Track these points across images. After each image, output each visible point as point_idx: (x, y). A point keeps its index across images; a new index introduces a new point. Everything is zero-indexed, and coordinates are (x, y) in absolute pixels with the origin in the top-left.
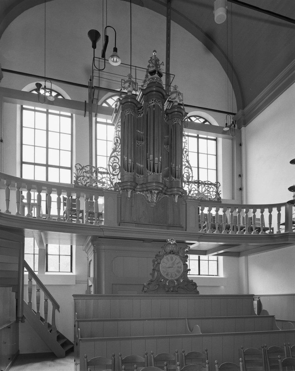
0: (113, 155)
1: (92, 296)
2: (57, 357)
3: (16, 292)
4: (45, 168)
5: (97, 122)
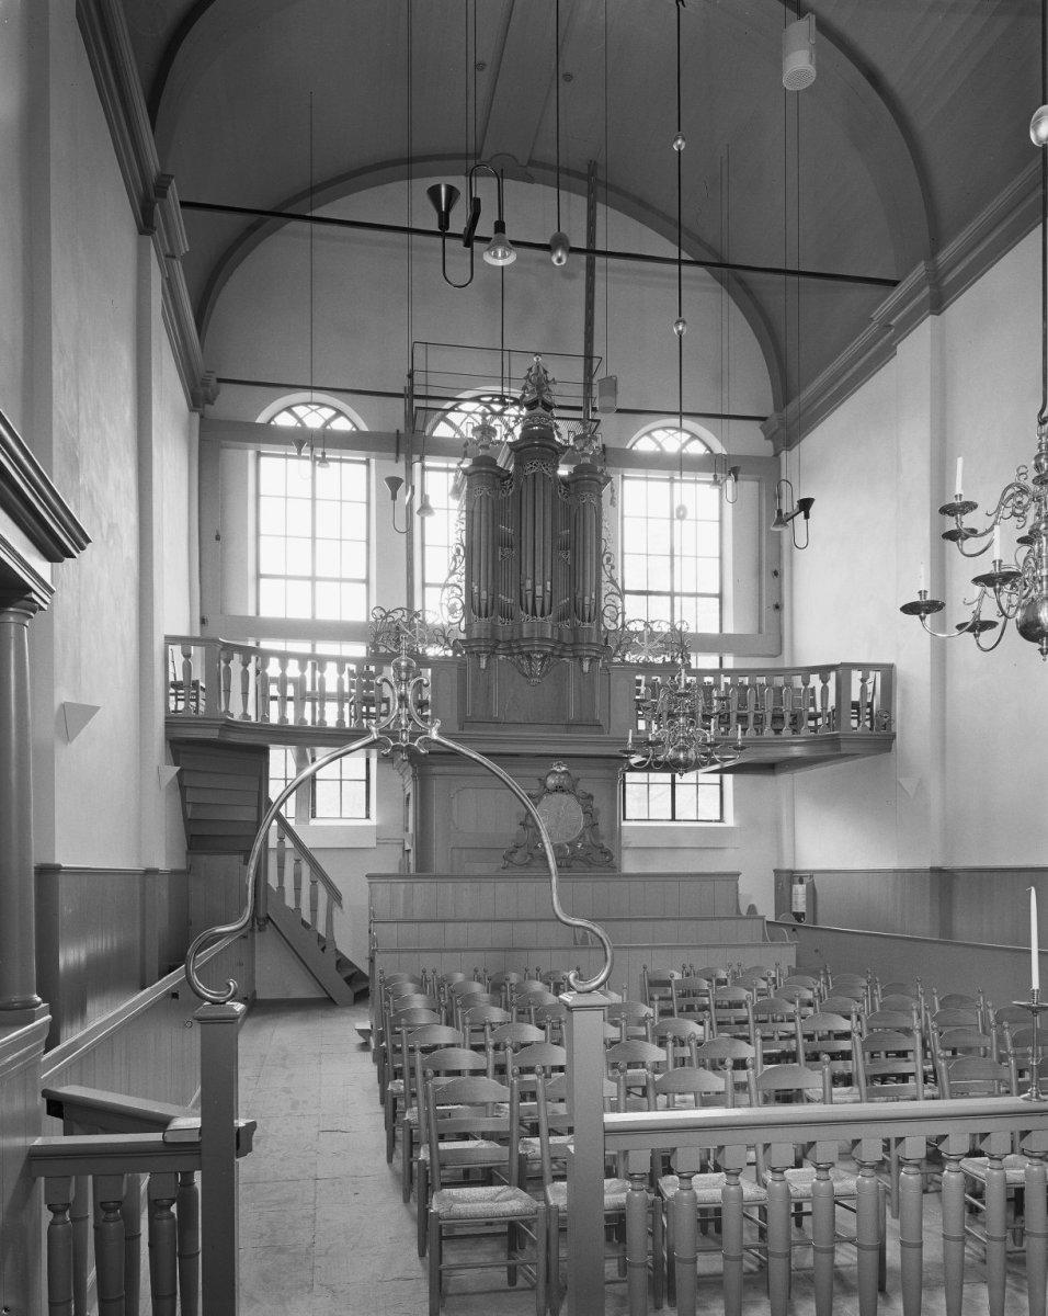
1: (410, 876)
2: (335, 1003)
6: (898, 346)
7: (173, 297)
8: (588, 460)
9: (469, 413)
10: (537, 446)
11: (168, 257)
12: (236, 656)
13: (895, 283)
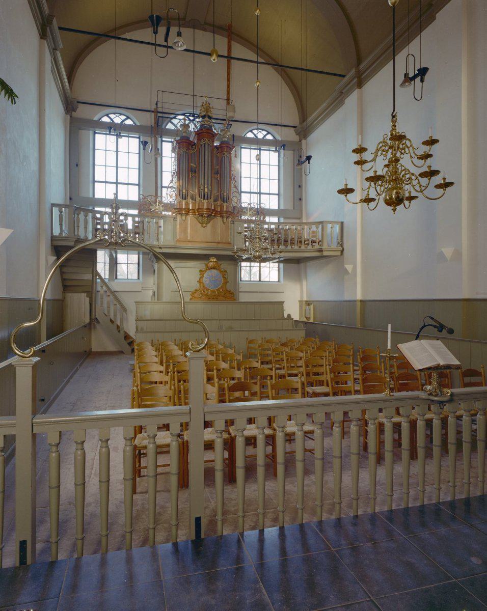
0: (171, 185)
3: (90, 298)
4: (119, 181)
5: (162, 141)
6: (346, 100)
7: (56, 65)
8: (226, 139)
9: (180, 120)
10: (205, 133)
11: (54, 50)
12: (82, 213)
13: (344, 76)
